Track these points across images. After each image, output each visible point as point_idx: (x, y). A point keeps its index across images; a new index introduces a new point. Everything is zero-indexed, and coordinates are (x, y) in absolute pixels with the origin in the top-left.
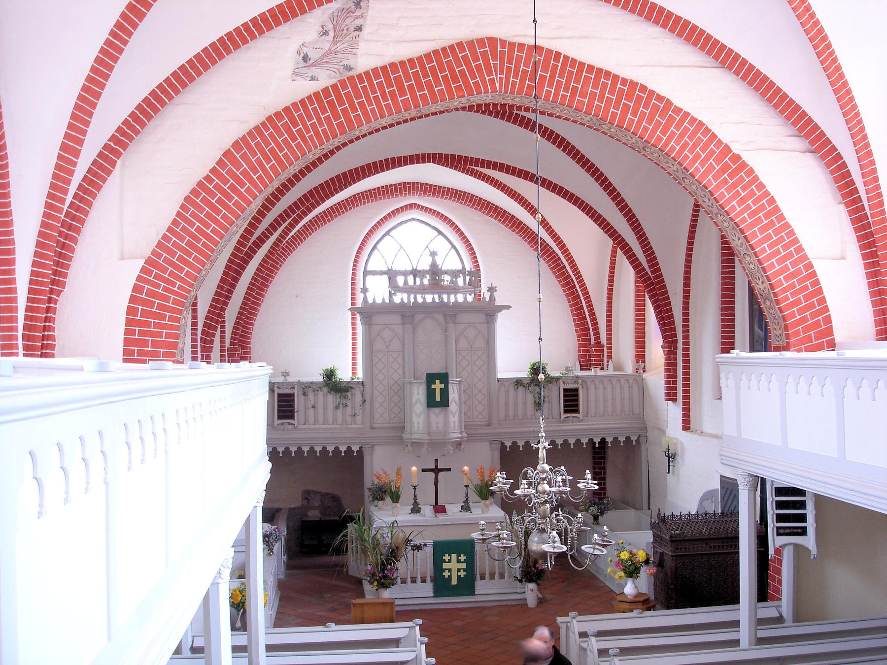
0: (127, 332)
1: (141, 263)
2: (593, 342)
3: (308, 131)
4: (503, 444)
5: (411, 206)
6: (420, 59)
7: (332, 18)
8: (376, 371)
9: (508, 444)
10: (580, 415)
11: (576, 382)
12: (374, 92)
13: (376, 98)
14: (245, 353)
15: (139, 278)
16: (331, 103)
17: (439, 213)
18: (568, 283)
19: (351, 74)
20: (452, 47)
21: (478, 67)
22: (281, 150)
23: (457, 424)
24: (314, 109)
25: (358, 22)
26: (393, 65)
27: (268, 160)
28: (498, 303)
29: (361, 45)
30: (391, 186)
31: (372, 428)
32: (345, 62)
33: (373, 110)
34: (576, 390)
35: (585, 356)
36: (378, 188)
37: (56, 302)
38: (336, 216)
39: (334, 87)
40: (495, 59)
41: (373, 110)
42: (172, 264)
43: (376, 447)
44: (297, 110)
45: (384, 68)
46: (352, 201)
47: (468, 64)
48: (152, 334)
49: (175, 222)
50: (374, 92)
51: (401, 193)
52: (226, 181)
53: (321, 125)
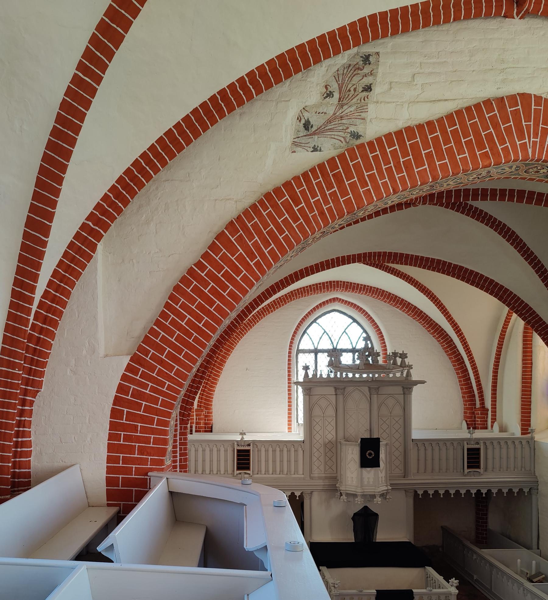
0: (111, 437)
1: (126, 360)
2: (478, 405)
3: (311, 210)
4: (416, 492)
5: (334, 300)
6: (440, 120)
7: (336, 77)
8: (314, 432)
9: (420, 492)
10: (481, 470)
11: (478, 443)
12: (387, 162)
13: (389, 170)
14: (208, 413)
15: (124, 378)
16: (337, 177)
17: (355, 305)
18: (458, 360)
19: (359, 142)
20: (477, 106)
21: (508, 130)
22: (281, 232)
23: (383, 479)
24: (319, 184)
25: (367, 81)
26: (409, 129)
27: (267, 244)
28: (414, 378)
29: (371, 108)
30: (320, 284)
31: (311, 478)
32: (352, 129)
33: (385, 184)
34: (479, 449)
35: (471, 417)
36: (310, 286)
37: (31, 403)
38: (277, 308)
39: (342, 156)
40: (528, 119)
41: (385, 184)
42: (161, 362)
43: (313, 493)
44: (300, 185)
45: (399, 133)
46: (290, 296)
47: (496, 126)
48: (138, 440)
49: (163, 315)
50: (387, 162)
51: (321, 291)
52: (219, 268)
53: (326, 202)
